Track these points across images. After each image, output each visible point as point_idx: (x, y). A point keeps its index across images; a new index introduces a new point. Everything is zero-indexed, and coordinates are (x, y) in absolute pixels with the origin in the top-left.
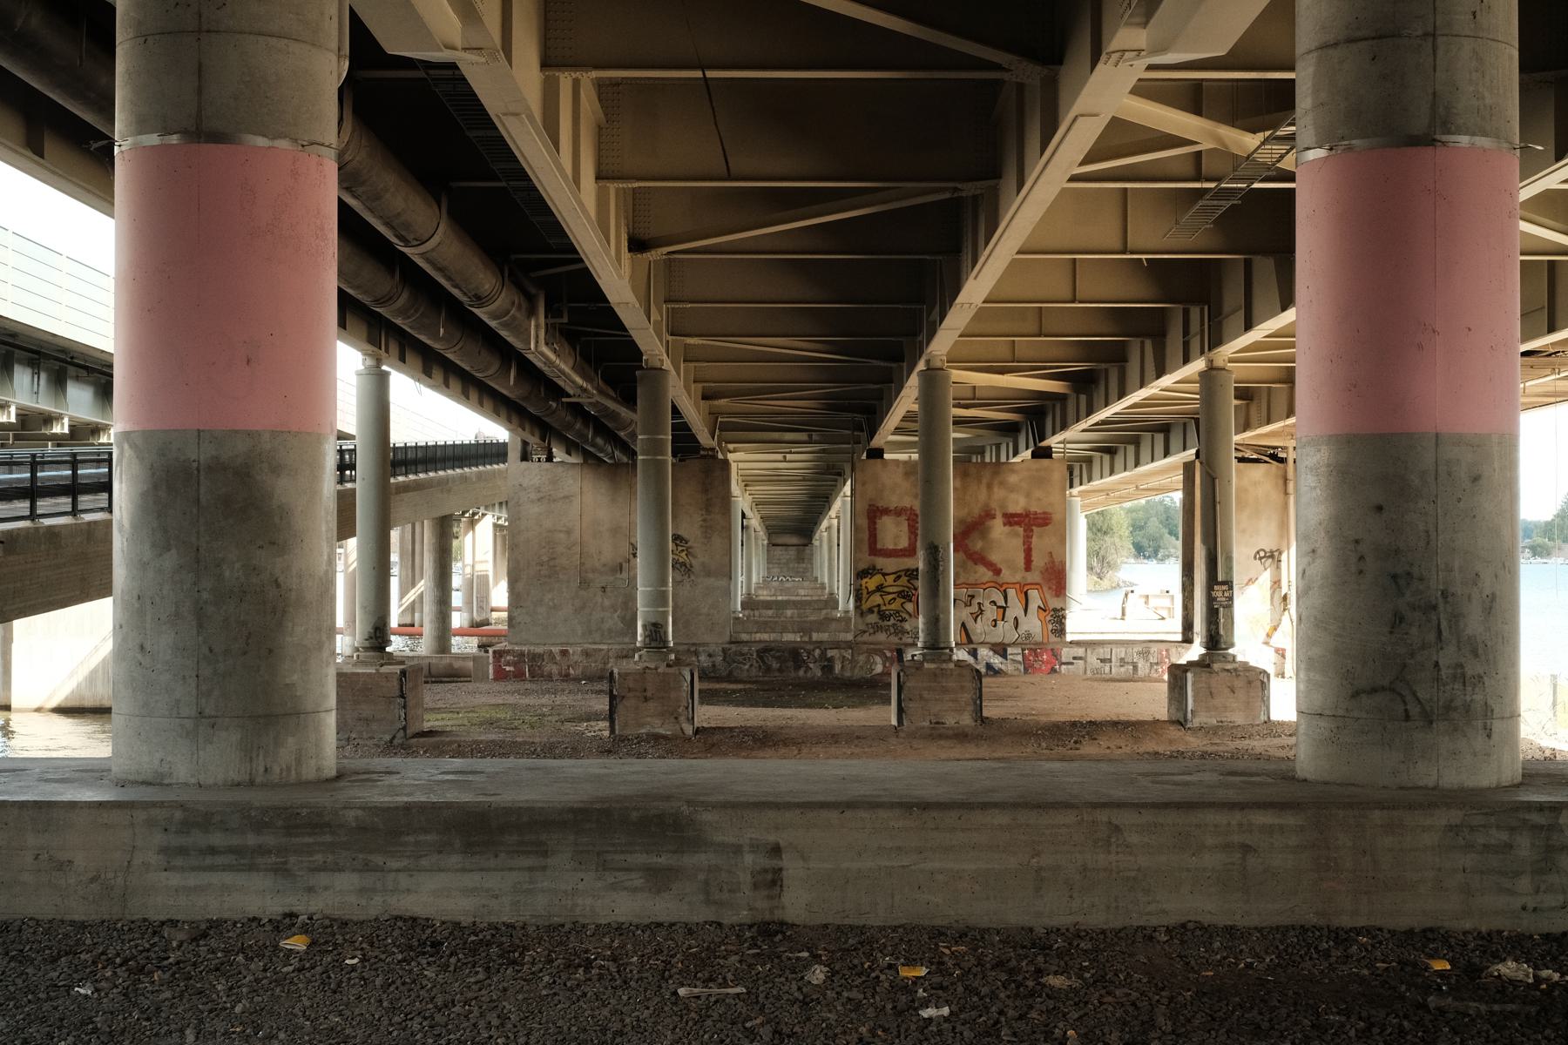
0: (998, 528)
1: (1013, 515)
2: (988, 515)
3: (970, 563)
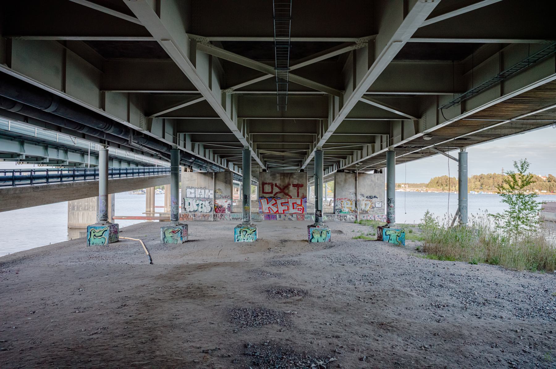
0: (291, 187)
1: (295, 185)
2: (289, 184)
3: (285, 195)
